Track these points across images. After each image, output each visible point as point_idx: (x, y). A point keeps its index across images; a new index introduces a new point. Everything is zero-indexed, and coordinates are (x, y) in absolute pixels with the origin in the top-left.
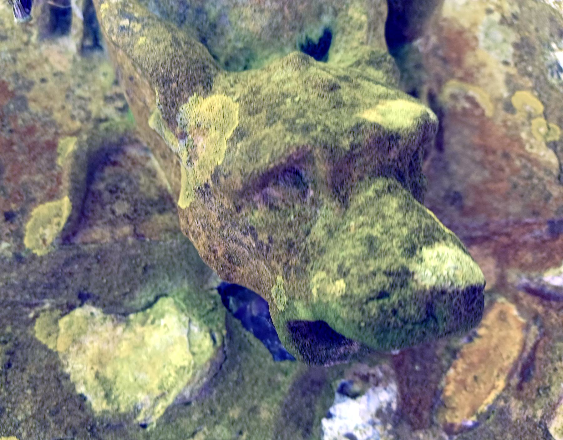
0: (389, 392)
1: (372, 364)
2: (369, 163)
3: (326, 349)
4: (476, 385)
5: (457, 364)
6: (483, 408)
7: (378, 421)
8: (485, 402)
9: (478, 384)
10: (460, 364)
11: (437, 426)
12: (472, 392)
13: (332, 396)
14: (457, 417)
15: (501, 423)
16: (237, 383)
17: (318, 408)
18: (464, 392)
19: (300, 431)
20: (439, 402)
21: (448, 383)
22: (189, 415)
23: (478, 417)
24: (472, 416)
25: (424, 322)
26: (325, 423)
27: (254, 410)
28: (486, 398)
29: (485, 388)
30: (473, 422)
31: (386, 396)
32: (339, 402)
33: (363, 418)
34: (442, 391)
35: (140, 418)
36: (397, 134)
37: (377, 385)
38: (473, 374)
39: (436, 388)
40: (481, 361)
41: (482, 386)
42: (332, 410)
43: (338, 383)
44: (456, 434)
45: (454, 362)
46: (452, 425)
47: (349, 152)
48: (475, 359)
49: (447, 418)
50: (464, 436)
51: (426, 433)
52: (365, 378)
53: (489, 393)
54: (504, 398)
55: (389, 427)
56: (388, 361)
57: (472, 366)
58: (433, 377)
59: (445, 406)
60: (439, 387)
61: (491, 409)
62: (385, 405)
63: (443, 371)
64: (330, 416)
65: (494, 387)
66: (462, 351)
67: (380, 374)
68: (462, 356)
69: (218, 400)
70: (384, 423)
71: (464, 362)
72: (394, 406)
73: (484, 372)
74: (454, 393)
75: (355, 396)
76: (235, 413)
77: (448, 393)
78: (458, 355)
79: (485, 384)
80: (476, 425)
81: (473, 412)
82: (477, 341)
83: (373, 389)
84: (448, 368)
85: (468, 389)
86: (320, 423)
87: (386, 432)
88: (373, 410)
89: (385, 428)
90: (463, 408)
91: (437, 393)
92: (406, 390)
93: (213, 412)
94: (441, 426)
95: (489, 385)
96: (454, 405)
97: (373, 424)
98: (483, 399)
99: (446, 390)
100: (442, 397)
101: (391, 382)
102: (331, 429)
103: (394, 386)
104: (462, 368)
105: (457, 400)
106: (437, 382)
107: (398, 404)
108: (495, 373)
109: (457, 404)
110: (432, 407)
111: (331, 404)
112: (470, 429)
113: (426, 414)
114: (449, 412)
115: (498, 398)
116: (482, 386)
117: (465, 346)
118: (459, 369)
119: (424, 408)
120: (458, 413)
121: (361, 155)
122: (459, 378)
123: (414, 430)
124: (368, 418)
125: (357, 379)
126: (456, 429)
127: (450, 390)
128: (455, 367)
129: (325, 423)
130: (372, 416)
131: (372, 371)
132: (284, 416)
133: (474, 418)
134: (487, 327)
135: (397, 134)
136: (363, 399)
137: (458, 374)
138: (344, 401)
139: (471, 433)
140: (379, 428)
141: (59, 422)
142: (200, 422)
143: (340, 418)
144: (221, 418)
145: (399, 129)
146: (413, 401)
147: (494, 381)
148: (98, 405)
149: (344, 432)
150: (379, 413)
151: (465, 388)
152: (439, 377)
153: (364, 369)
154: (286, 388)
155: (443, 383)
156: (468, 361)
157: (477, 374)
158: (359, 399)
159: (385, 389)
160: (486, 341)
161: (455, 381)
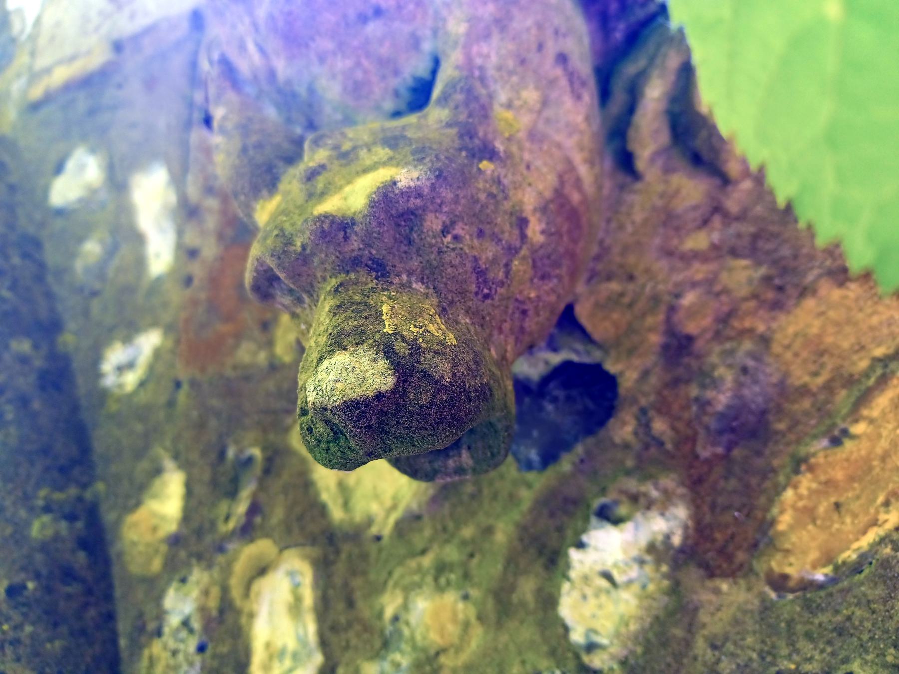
0: (668, 520)
1: (646, 477)
2: (326, 261)
3: (430, 462)
4: (835, 517)
5: (799, 482)
6: (850, 555)
7: (648, 558)
8: (855, 545)
9: (840, 516)
10: (806, 483)
11: (757, 575)
12: (822, 528)
13: (587, 520)
14: (791, 565)
15: (885, 582)
16: (473, 497)
17: (569, 533)
18: (810, 527)
19: (542, 560)
20: (766, 540)
21: (782, 512)
22: (421, 530)
23: (837, 568)
24: (824, 566)
25: (336, 439)
26: (574, 554)
27: (488, 531)
28: (857, 540)
29: (853, 523)
30: (826, 575)
31: (666, 524)
32: (595, 528)
33: (625, 551)
34: (773, 523)
35: (374, 530)
36: (352, 219)
37: (648, 507)
38: (833, 499)
39: (764, 518)
40: (851, 479)
41: (848, 520)
42: (585, 538)
43: (597, 503)
44: (793, 591)
45: (795, 478)
46: (785, 577)
47: (300, 254)
48: (839, 475)
49: (774, 564)
50: (809, 595)
51: (736, 583)
52: (634, 499)
53: (864, 532)
54: (892, 542)
55: (665, 568)
56: (674, 476)
57: (829, 484)
58: (762, 500)
59: (774, 547)
60: (769, 517)
61: (864, 558)
62: (660, 538)
63: (779, 490)
64: (581, 545)
65: (874, 523)
66: (813, 460)
67: (655, 494)
68: (811, 469)
69: (452, 515)
70: (658, 562)
71: (815, 479)
72: (677, 540)
73: (858, 497)
74: (792, 527)
75: (617, 521)
76: (468, 532)
77: (781, 527)
78: (803, 467)
79: (855, 516)
80: (833, 580)
81: (828, 558)
82: (848, 444)
83: (643, 514)
84: (784, 489)
85: (819, 522)
86: (566, 555)
87: (658, 576)
88: (643, 541)
89: (657, 570)
90: (805, 552)
91: (766, 525)
92: (708, 518)
93: (445, 529)
94: (762, 575)
95: (864, 519)
96: (787, 546)
97: (641, 562)
98: (851, 542)
99: (779, 522)
100: (771, 533)
101: (675, 505)
102: (581, 562)
103: (681, 512)
104: (809, 489)
105: (794, 538)
106: (767, 509)
107: (686, 537)
108: (881, 499)
109: (793, 544)
110: (755, 545)
111: (584, 530)
112: (821, 586)
113: (741, 556)
114: (779, 556)
115: (882, 541)
116: (848, 520)
117: (821, 455)
118: (803, 491)
119: (739, 548)
120: (792, 559)
121: (313, 254)
122: (801, 504)
123: (711, 575)
124: (634, 553)
125: (624, 498)
126: (792, 584)
127: (785, 521)
128: (795, 487)
129: (574, 554)
130: (640, 550)
131: (643, 489)
132: (521, 540)
133: (828, 570)
134: (871, 421)
135: (352, 219)
136: (629, 526)
137: (800, 497)
138: (602, 527)
139: (822, 593)
140: (649, 569)
141: (302, 529)
142: (431, 540)
143: (596, 549)
144: (453, 536)
145: (355, 213)
146: (718, 536)
147: (877, 512)
148: (337, 514)
149: (599, 568)
150: (651, 548)
151: (814, 521)
152: (771, 501)
153: (632, 485)
154: (526, 505)
155: (775, 511)
156: (823, 478)
157: (842, 499)
158: (622, 526)
159: (662, 514)
160: (865, 445)
161: (794, 507)
